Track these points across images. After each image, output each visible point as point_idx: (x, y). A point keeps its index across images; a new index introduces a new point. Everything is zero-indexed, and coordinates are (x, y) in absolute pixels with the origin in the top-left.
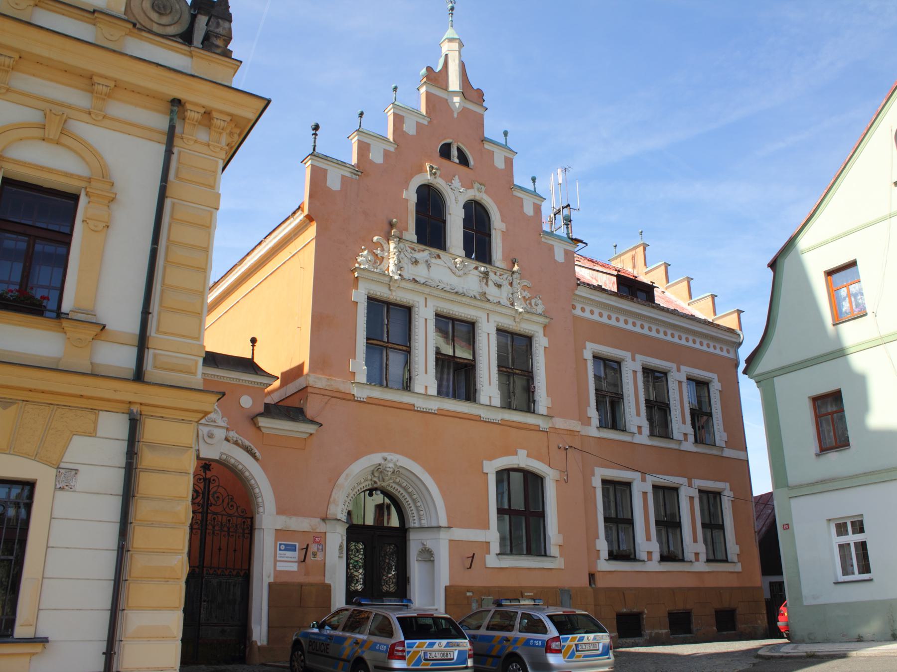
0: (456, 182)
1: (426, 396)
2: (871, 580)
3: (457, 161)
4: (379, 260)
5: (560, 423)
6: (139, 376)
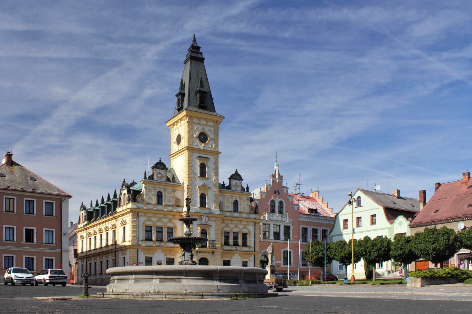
0: (277, 198)
1: (272, 240)
2: (342, 271)
3: (277, 194)
4: (264, 217)
5: (294, 242)
6: (255, 251)
